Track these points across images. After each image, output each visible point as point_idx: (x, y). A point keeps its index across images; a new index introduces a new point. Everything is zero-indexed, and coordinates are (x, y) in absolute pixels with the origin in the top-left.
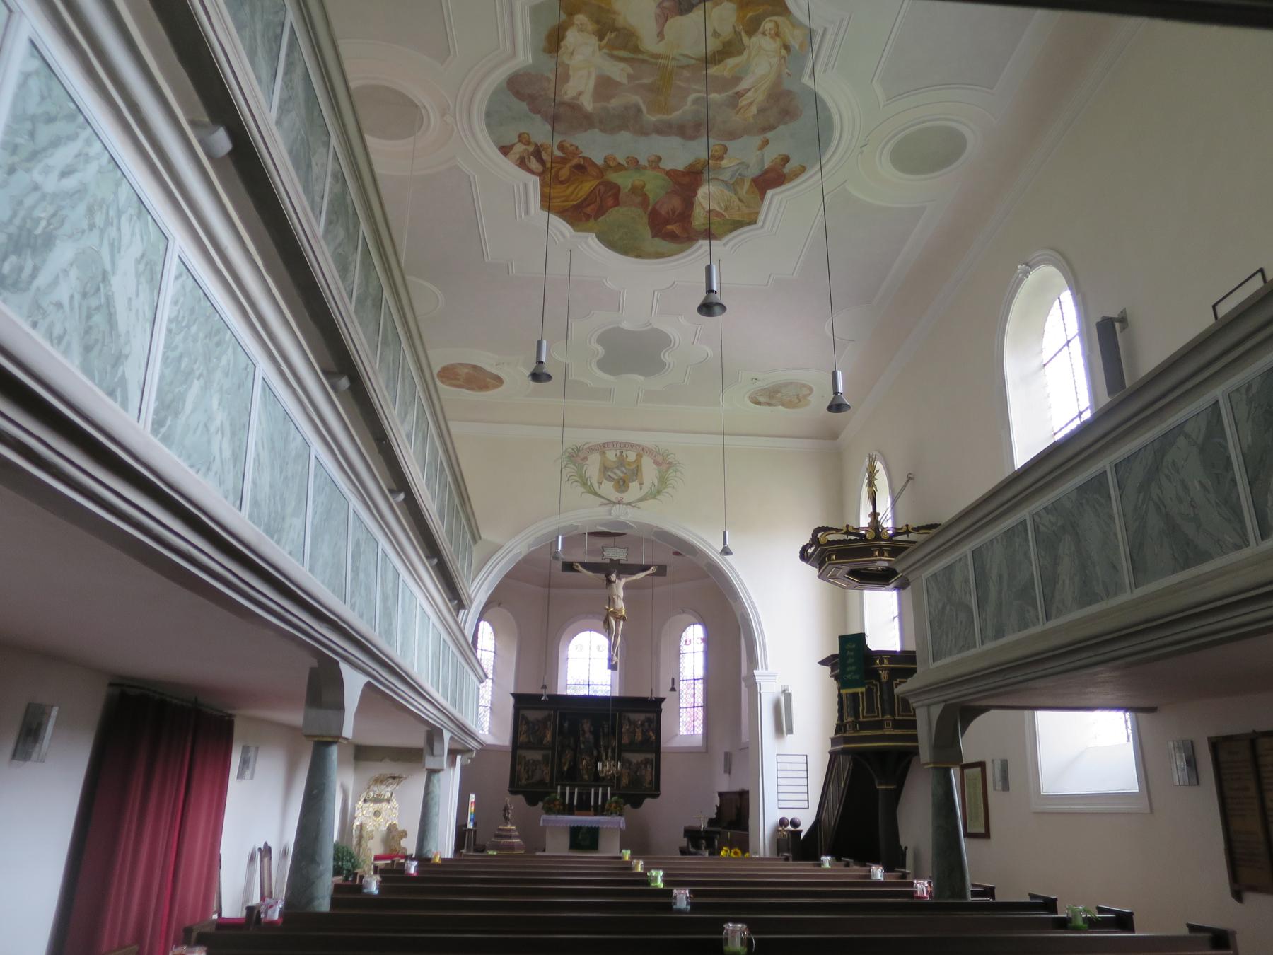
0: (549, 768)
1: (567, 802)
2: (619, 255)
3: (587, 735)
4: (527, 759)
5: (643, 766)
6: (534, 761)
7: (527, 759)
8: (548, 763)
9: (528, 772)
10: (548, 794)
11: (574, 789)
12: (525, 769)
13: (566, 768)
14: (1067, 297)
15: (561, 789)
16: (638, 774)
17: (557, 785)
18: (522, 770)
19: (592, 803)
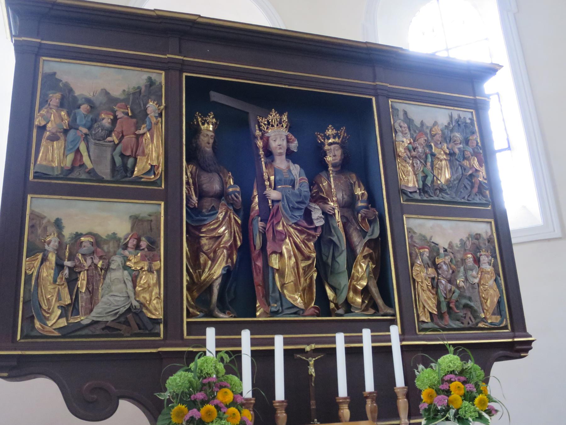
0: (160, 264)
1: (369, 386)
2: (9, 382)
3: (281, 163)
4: (67, 233)
5: (422, 287)
6: (97, 241)
7: (67, 233)
8: (153, 245)
9: (72, 281)
10: (191, 356)
11: (272, 342)
12: (60, 267)
13: (218, 270)
14: (290, 161)
15: (253, 342)
16: (460, 281)
17: (200, 328)
18: (48, 273)
19: (343, 391)
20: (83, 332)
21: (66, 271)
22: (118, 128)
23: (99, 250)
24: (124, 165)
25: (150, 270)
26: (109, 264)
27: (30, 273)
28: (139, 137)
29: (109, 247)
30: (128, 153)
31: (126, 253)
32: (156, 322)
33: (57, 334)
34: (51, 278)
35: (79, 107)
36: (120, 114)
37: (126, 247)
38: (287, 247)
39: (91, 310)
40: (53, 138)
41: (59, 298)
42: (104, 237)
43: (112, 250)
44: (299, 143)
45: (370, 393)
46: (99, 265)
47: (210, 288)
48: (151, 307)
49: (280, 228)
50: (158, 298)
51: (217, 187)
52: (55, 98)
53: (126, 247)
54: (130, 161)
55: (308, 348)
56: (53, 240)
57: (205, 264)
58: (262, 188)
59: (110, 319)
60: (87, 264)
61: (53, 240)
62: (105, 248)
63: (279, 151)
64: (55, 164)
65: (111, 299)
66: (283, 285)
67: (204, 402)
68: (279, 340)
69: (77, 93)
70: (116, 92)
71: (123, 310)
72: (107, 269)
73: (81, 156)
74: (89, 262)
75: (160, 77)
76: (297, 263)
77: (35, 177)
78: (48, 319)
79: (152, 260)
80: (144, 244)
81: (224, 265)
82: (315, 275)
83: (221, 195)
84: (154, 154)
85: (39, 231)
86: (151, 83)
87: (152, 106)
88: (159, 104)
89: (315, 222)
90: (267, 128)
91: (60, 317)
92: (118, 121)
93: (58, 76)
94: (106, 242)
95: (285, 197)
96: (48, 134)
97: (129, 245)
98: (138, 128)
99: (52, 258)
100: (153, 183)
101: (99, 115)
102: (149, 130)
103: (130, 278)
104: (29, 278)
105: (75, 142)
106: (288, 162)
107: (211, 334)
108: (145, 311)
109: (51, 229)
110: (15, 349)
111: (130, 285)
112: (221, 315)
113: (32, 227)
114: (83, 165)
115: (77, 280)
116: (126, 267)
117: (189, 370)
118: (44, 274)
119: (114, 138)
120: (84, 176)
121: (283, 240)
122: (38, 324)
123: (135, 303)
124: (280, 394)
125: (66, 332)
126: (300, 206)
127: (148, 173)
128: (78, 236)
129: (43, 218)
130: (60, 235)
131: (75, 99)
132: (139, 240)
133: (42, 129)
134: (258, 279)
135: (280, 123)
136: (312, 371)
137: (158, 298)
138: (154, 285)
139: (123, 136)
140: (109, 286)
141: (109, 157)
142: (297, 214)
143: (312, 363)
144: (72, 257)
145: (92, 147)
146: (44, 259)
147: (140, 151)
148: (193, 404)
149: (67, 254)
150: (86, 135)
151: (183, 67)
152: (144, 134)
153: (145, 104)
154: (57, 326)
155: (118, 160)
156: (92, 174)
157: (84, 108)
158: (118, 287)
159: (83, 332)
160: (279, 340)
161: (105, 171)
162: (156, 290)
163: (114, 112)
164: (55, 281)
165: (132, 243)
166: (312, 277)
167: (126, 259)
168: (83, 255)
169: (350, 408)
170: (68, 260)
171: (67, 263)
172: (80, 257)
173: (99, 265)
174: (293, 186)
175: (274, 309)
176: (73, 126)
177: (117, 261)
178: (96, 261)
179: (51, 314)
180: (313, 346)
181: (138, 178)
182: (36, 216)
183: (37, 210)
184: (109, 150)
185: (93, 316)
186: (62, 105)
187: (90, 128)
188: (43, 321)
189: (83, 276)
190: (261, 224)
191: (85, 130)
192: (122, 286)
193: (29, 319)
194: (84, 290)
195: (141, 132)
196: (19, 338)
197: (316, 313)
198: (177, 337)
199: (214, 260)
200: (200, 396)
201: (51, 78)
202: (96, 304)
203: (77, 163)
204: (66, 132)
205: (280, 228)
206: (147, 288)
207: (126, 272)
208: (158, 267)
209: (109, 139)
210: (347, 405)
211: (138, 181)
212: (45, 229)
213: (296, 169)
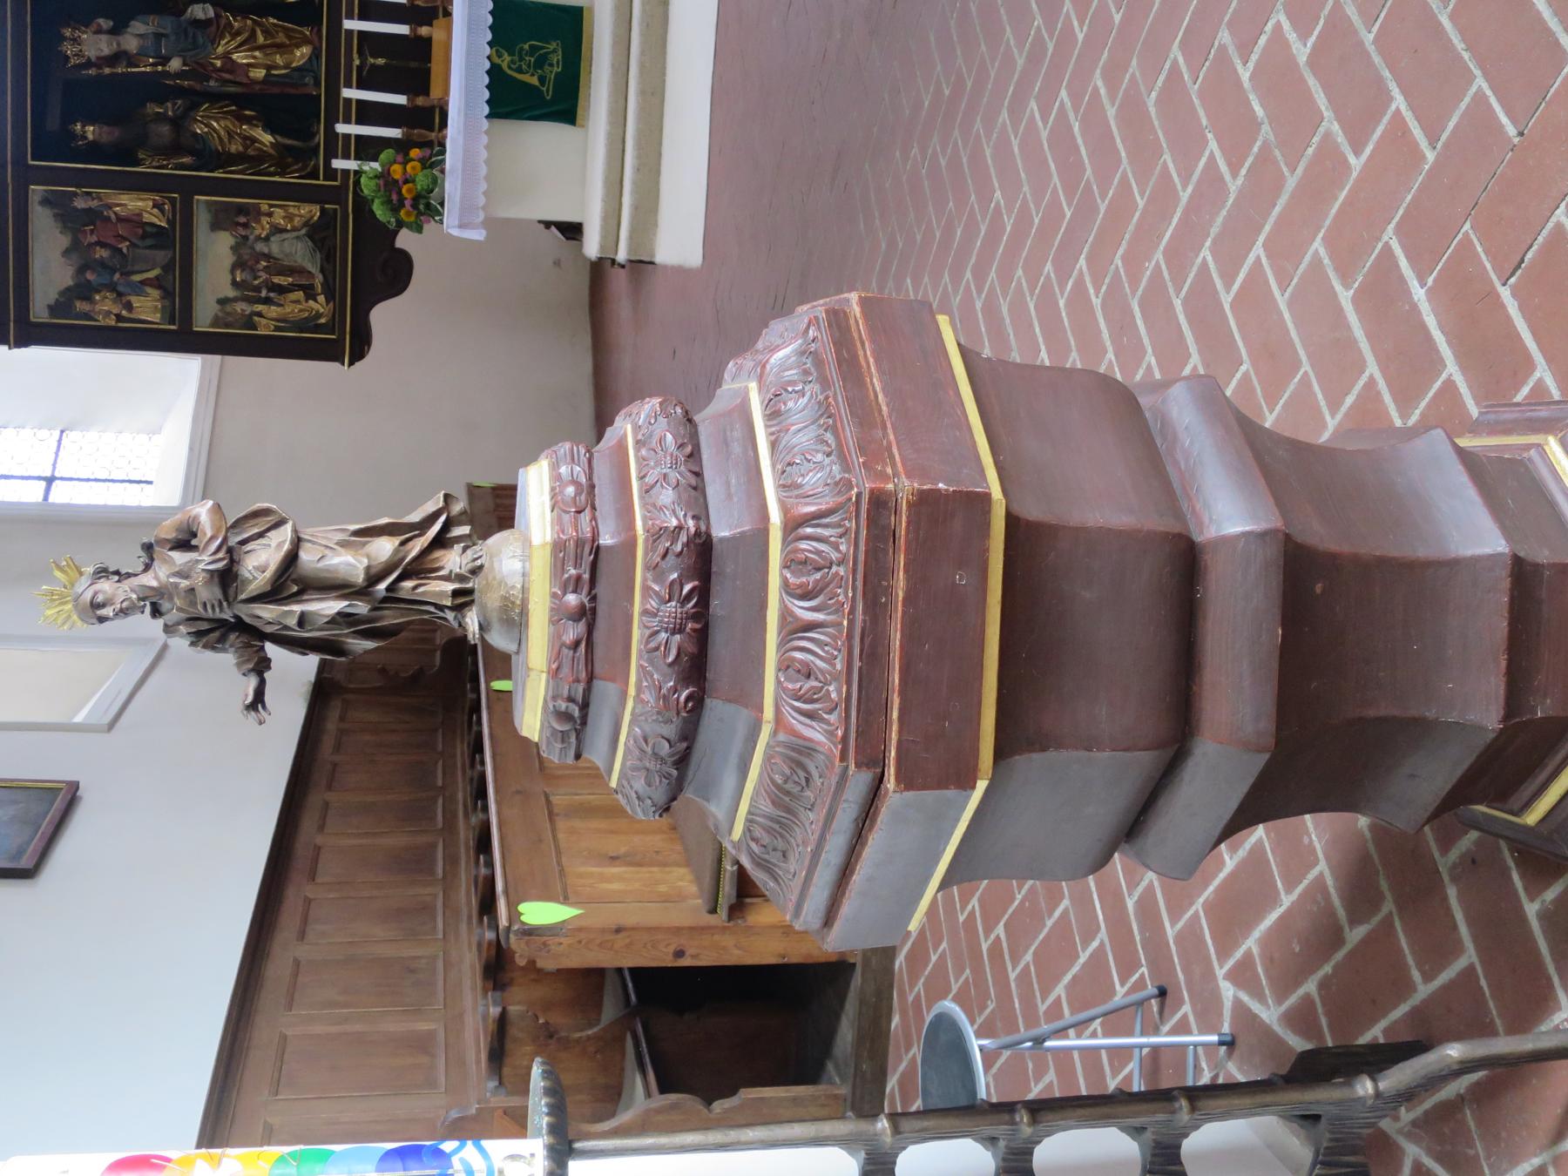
0: (264, 205)
6: (239, 264)
8: (241, 210)
9: (281, 290)
12: (267, 301)
13: (267, 138)
17: (331, 173)
18: (273, 311)
19: (403, 29)
20: (331, 282)
21: (272, 295)
22: (111, 241)
23: (250, 263)
24: (152, 235)
25: (270, 215)
26: (264, 255)
27: (272, 327)
28: (120, 219)
29: (245, 252)
30: (140, 231)
31: (252, 237)
32: (323, 211)
33: (331, 304)
34: (279, 309)
35: (89, 281)
36: (94, 239)
37: (246, 238)
38: (240, 58)
39: (310, 272)
40: (129, 307)
41: (297, 302)
42: (235, 258)
43: (249, 251)
44: (102, 17)
45: (411, 29)
46: (264, 264)
47: (287, 147)
48: (308, 216)
49: (218, 63)
50: (299, 208)
51: (165, 129)
52: (81, 306)
53: (246, 238)
54: (149, 229)
55: (357, 62)
56: (240, 307)
57: (259, 149)
58: (166, 74)
59: (318, 255)
60: (264, 276)
61: (240, 307)
62: (246, 257)
63: (115, 44)
64: (159, 305)
65: (299, 254)
66: (285, 67)
67: (400, 193)
68: (348, 93)
69: (70, 283)
70: (64, 241)
71: (310, 243)
72: (267, 257)
73: (148, 279)
74: (261, 274)
75: (37, 190)
76: (259, 48)
77: (174, 324)
78: (317, 312)
79: (258, 213)
80: (242, 220)
81: (260, 131)
82: (272, 20)
83: (178, 123)
84: (140, 204)
85: (230, 319)
86: (46, 202)
87: (80, 204)
88: (75, 194)
89: (208, 17)
90: (83, 57)
91: (316, 301)
92: (102, 239)
93: (52, 302)
94: (239, 257)
95: (181, 53)
96: (124, 313)
97: (243, 233)
98: (108, 219)
99: (259, 308)
100: (174, 207)
101: (95, 260)
102: (110, 208)
103: (278, 235)
104: (277, 329)
105: (132, 285)
106: (126, 32)
107: (338, 164)
108: (312, 222)
109: (228, 308)
110: (345, 339)
111: (285, 236)
112: (317, 140)
113: (227, 326)
114: (157, 278)
115: (279, 285)
116: (267, 239)
117: (373, 201)
118: (274, 315)
119: (124, 246)
120: (171, 277)
121: (233, 61)
122: (323, 321)
123: (304, 231)
124: (400, 99)
125: (330, 295)
126: (191, 35)
127: (162, 211)
128: (234, 283)
129: (216, 315)
130: (235, 300)
131: (77, 285)
132: (238, 224)
133: (119, 318)
134: (276, 90)
135: (74, 40)
136: (381, 61)
137: (299, 208)
138: (286, 211)
139: (119, 236)
140: (287, 255)
141: (147, 251)
142: (201, 40)
143: (372, 61)
144: (258, 289)
145: (137, 268)
146: (260, 315)
147: (135, 218)
148: (401, 204)
149: (254, 294)
150: (122, 274)
151: (19, 161)
152: (115, 213)
153: (76, 209)
154: (324, 304)
155: (149, 242)
156: (168, 268)
157: (90, 276)
158: (287, 247)
159: (331, 282)
160: (348, 93)
161: (161, 256)
162: (291, 210)
163: (91, 245)
164: (281, 305)
165: (242, 232)
166: (274, 25)
167: (258, 238)
168: (255, 279)
169: (421, 26)
170: (260, 292)
171: (264, 293)
172: (256, 282)
173: (264, 264)
174: (163, 35)
175: (312, 82)
176: (112, 287)
177: (261, 247)
178: (261, 267)
179: (313, 309)
180: (355, 56)
181: (168, 221)
182: (216, 322)
183: (208, 321)
184: (138, 251)
185: (315, 270)
186: (88, 298)
187: (114, 271)
188: (319, 315)
189: (276, 280)
190: (212, 83)
191: (117, 276)
192: (286, 243)
193: (318, 328)
194: (290, 279)
195: (113, 216)
196: (334, 337)
197: (489, 923)
198: (337, 195)
199: (254, 140)
200: (394, 197)
201: (53, 310)
202: (304, 268)
203: (157, 283)
204: (120, 295)
205: (218, 63)
206: (289, 218)
207: (272, 239)
208: (266, 207)
209: (125, 250)
210: (419, 29)
211: (171, 222)
212: (228, 314)
213: (138, 27)
